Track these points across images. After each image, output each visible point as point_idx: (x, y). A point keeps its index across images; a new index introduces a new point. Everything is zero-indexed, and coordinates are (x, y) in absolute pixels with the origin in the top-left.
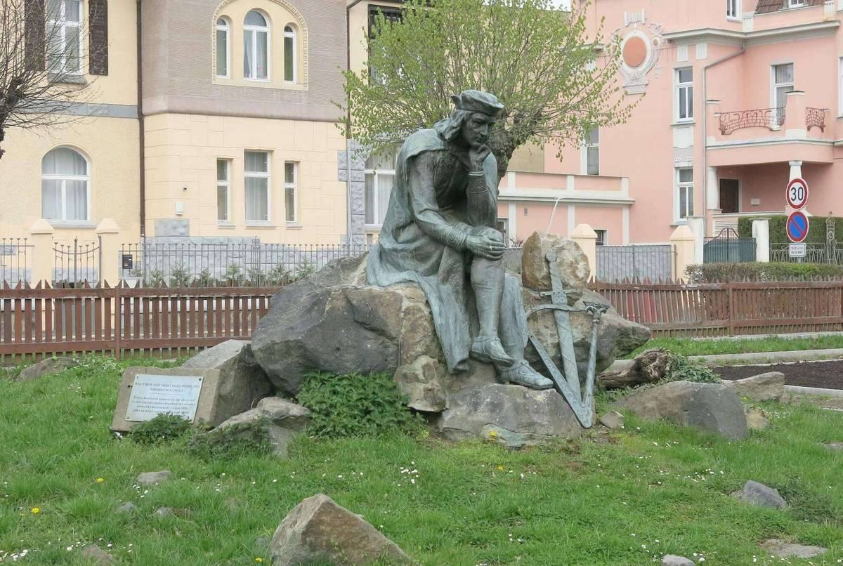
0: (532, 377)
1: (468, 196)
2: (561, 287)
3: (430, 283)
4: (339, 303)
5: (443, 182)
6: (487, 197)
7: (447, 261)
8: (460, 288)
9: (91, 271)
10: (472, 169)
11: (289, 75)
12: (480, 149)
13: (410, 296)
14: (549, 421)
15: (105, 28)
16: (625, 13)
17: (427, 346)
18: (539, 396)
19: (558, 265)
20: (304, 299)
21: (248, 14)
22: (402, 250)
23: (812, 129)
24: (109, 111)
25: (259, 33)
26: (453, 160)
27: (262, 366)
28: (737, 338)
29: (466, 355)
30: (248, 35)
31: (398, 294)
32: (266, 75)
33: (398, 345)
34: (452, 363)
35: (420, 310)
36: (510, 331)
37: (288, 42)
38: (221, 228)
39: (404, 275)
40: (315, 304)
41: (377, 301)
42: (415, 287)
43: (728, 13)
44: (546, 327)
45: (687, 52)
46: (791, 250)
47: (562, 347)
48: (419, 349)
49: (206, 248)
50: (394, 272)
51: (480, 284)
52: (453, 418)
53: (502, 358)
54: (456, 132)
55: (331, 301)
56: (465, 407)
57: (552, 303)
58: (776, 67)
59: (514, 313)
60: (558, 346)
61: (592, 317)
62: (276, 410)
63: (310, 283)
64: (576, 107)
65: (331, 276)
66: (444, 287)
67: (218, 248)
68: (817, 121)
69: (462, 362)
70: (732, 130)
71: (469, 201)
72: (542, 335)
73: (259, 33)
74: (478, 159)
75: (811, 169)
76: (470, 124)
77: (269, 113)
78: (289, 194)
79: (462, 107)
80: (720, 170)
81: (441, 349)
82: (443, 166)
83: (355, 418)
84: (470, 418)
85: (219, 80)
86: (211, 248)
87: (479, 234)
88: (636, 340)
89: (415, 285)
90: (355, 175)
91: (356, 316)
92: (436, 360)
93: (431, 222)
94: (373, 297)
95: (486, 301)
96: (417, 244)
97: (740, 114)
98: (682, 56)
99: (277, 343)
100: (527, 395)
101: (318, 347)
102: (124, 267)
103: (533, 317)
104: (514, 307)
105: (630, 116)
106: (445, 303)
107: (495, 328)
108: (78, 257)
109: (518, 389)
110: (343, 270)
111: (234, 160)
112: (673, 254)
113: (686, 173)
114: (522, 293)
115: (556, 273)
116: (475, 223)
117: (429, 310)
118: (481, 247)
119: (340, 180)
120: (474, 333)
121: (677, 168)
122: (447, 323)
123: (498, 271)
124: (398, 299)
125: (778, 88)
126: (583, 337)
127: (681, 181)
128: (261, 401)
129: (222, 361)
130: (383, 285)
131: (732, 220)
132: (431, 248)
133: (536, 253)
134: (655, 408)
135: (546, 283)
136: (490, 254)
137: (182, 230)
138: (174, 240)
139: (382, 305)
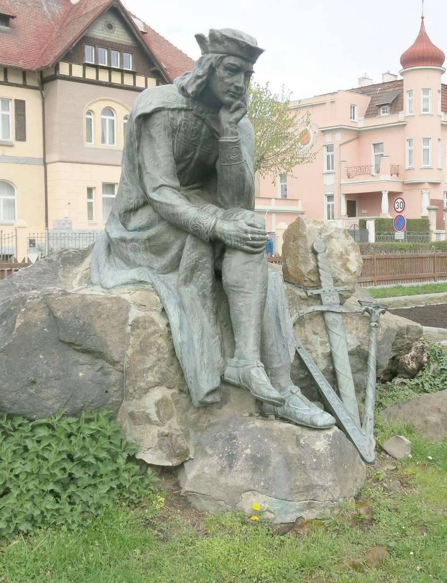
0: (307, 413)
1: (219, 171)
2: (331, 283)
3: (169, 284)
4: (36, 315)
5: (186, 152)
6: (242, 170)
7: (191, 253)
8: (208, 291)
9: (10, 248)
12: (234, 106)
13: (139, 302)
15: (24, 115)
17: (163, 374)
18: (318, 443)
19: (327, 257)
21: (102, 111)
22: (132, 240)
24: (28, 161)
26: (199, 123)
28: (378, 287)
29: (216, 383)
30: (103, 121)
31: (124, 300)
32: (114, 142)
33: (123, 372)
34: (197, 394)
35: (153, 322)
36: (274, 348)
38: (90, 224)
39: (133, 274)
41: (92, 311)
42: (147, 290)
43: (351, 118)
44: (315, 333)
46: (396, 236)
47: (335, 358)
48: (151, 378)
49: (81, 235)
55: (24, 313)
56: (216, 458)
57: (321, 304)
58: (374, 145)
59: (278, 319)
60: (330, 357)
61: (369, 319)
63: (12, 284)
64: (285, 152)
65: (44, 273)
67: (88, 235)
68: (395, 172)
69: (213, 392)
71: (219, 177)
72: (311, 343)
74: (231, 120)
75: (392, 195)
76: (220, 72)
79: (210, 49)
80: (347, 195)
81: (182, 375)
82: (185, 131)
84: (223, 480)
85: (88, 145)
86: (85, 235)
87: (232, 218)
88: (409, 339)
89: (147, 286)
91: (61, 334)
92: (175, 391)
93: (168, 202)
94: (87, 305)
95: (243, 309)
96: (152, 232)
98: (328, 139)
100: (302, 441)
102: (30, 246)
103: (300, 322)
104: (277, 311)
105: (315, 158)
106: (188, 312)
107: (256, 348)
108: (3, 240)
109: (288, 429)
113: (330, 198)
114: (288, 293)
115: (326, 267)
117: (165, 322)
118: (237, 236)
120: (228, 352)
121: (325, 195)
122: (191, 339)
123: (259, 268)
124: (123, 307)
125: (375, 155)
126: (359, 344)
127: (328, 201)
130: (112, 286)
131: (355, 220)
132: (169, 236)
133: (300, 243)
134: (440, 423)
135: (314, 278)
136: (247, 245)
137: (68, 226)
138: (63, 231)
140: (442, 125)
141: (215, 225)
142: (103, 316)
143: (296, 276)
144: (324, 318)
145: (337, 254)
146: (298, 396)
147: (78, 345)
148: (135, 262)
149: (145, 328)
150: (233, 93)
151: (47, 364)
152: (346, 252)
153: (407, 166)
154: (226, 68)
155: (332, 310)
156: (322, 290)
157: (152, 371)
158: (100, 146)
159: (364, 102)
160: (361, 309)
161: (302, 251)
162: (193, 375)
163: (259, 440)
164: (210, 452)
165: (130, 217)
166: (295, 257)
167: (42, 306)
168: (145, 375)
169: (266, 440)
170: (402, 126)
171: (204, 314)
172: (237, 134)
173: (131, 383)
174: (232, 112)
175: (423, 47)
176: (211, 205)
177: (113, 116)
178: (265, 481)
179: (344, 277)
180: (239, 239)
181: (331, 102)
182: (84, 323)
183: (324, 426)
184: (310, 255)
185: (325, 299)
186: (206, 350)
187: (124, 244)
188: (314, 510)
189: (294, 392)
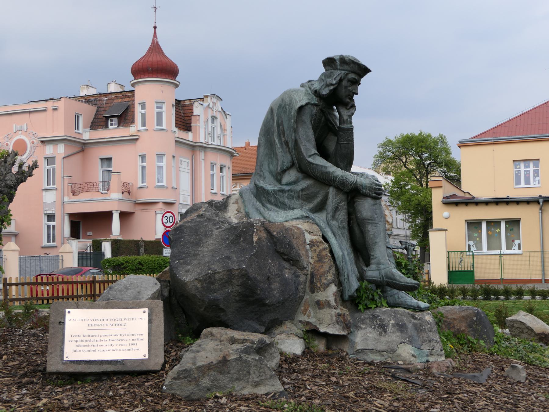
16: (14, 125)
22: (289, 190)
33: (306, 275)
45: (52, 147)
51: (369, 220)
53: (411, 283)
76: (344, 83)
79: (338, 67)
80: (71, 215)
98: (49, 150)
99: (219, 273)
112: (61, 260)
113: (51, 217)
118: (370, 187)
121: (45, 214)
124: (302, 233)
127: (48, 221)
140: (176, 141)
147: (287, 255)
148: (290, 206)
151: (273, 266)
153: (140, 184)
159: (89, 111)
164: (363, 326)
168: (326, 275)
170: (134, 140)
175: (154, 58)
178: (408, 337)
180: (371, 189)
181: (53, 109)
187: (281, 194)
188: (433, 356)
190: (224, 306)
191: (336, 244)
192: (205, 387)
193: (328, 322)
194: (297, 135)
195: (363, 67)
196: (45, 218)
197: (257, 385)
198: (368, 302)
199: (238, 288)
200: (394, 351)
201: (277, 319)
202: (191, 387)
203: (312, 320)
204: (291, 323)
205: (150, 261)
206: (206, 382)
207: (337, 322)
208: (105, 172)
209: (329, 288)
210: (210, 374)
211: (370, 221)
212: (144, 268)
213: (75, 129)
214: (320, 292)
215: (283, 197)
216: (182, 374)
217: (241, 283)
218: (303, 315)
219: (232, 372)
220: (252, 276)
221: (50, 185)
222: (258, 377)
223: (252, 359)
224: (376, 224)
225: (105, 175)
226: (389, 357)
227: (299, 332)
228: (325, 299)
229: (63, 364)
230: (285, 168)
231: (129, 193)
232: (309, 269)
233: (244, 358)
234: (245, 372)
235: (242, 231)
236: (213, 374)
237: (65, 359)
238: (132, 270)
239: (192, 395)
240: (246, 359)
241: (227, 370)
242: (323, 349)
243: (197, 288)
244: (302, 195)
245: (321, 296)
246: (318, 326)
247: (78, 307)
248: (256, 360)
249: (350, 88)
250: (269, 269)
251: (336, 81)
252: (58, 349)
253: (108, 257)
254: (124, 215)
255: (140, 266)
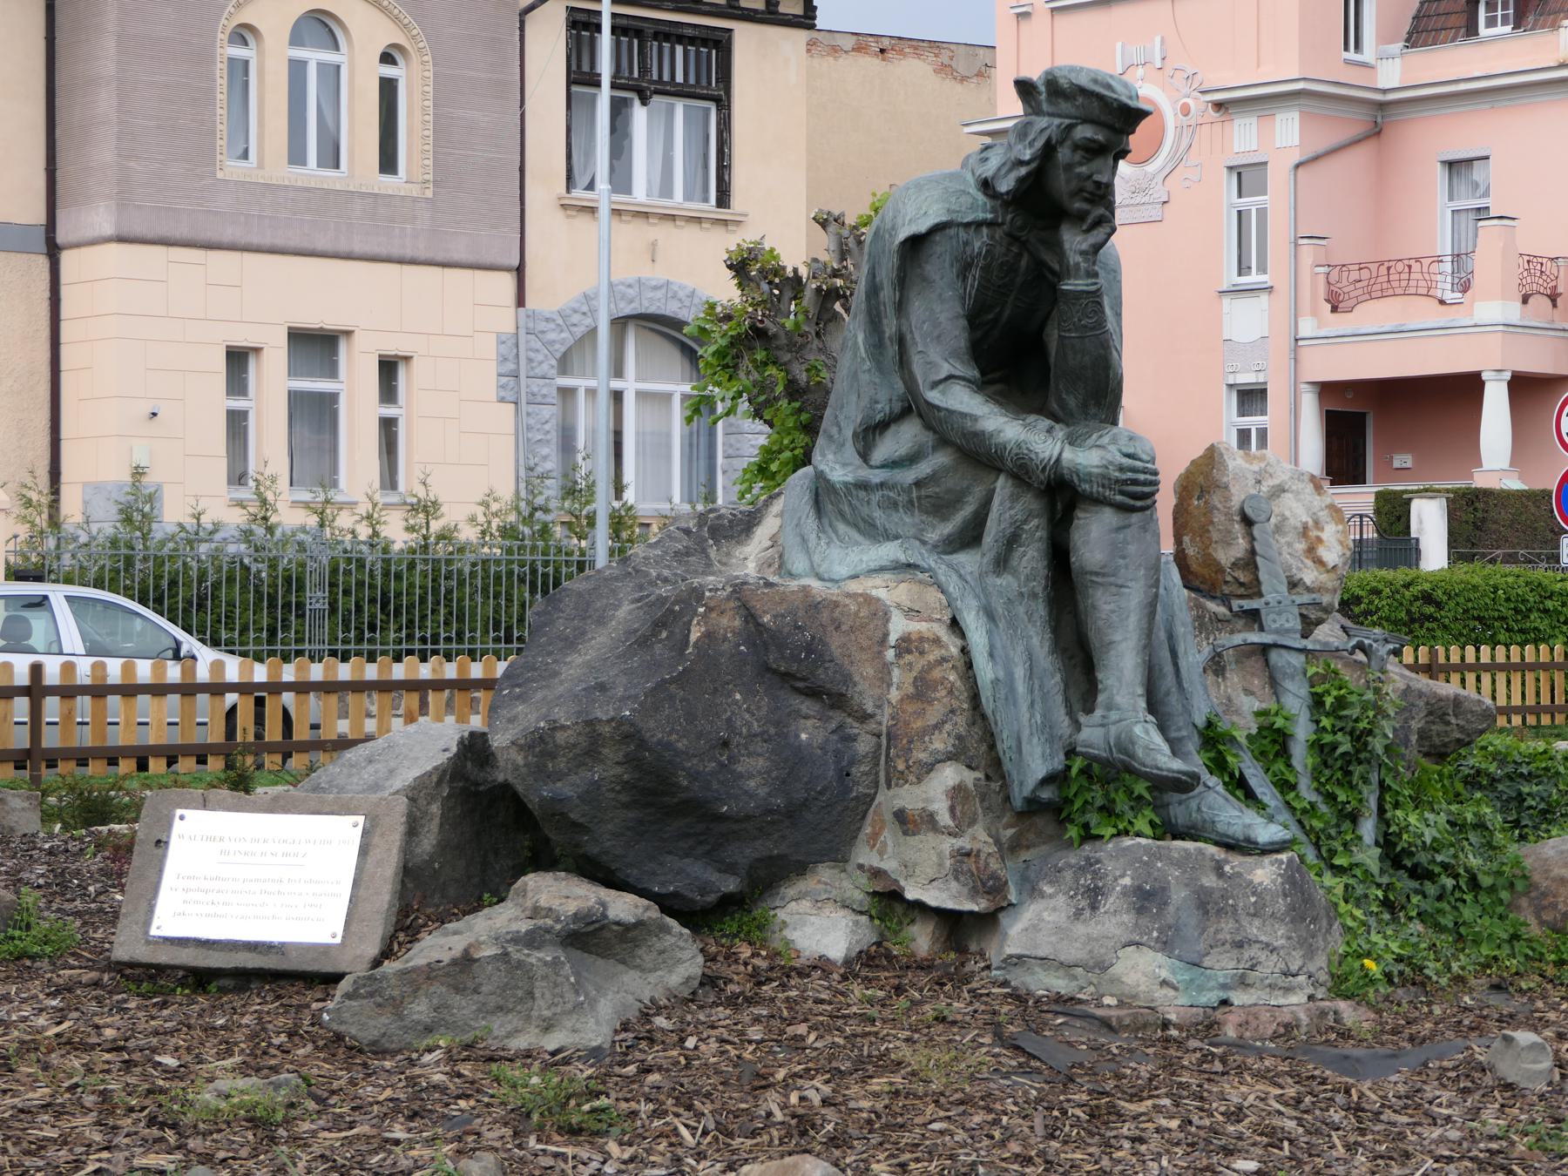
2: (1284, 588)
4: (724, 621)
8: (1039, 586)
10: (1066, 272)
11: (388, 163)
13: (907, 603)
14: (1289, 938)
16: (1119, 45)
17: (959, 738)
18: (1259, 872)
20: (625, 612)
22: (882, 485)
23: (1531, 300)
25: (321, 66)
27: (520, 789)
30: (297, 69)
31: (878, 600)
33: (879, 736)
34: (1021, 784)
35: (937, 641)
37: (388, 89)
39: (889, 551)
40: (659, 624)
41: (825, 615)
45: (1254, 127)
48: (940, 743)
50: (857, 544)
51: (1097, 574)
52: (1034, 928)
53: (1169, 770)
54: (1028, 175)
55: (704, 616)
57: (1262, 629)
58: (1451, 165)
62: (571, 907)
63: (637, 571)
66: (999, 581)
70: (1354, 301)
73: (321, 66)
74: (1084, 247)
75: (1525, 388)
76: (1064, 154)
77: (343, 247)
78: (388, 426)
79: (1045, 107)
80: (1327, 390)
83: (1416, 866)
85: (232, 169)
88: (1461, 728)
90: (535, 389)
92: (979, 775)
96: (924, 469)
97: (1373, 267)
98: (1244, 137)
99: (563, 728)
100: (1227, 868)
101: (674, 737)
103: (1216, 665)
110: (717, 542)
111: (265, 350)
113: (1251, 398)
116: (1072, 415)
118: (1103, 476)
119: (502, 400)
121: (1231, 386)
122: (1010, 675)
124: (881, 614)
127: (1242, 413)
128: (519, 883)
129: (409, 775)
131: (1360, 498)
133: (1216, 500)
135: (1243, 577)
136: (1122, 493)
139: (837, 628)
141: (1060, 454)
142: (844, 628)
143: (1205, 572)
144: (1267, 661)
145: (1296, 528)
146: (1218, 793)
147: (804, 679)
148: (886, 530)
149: (922, 653)
150: (1091, 193)
151: (748, 710)
152: (1317, 523)
154: (1076, 147)
155: (1285, 643)
156: (1263, 600)
157: (941, 732)
158: (279, 171)
160: (1347, 643)
161: (1218, 518)
162: (1014, 745)
163: (1146, 863)
164: (1048, 890)
165: (874, 439)
166: (1204, 531)
167: (732, 604)
168: (927, 739)
169: (1159, 865)
171: (1032, 631)
172: (1096, 275)
173: (900, 753)
174: (1088, 230)
176: (1036, 417)
177: (337, 47)
178: (1160, 931)
179: (1310, 576)
180: (1106, 482)
182: (813, 638)
183: (1272, 843)
184: (1237, 526)
185: (1267, 619)
186: (1038, 700)
187: (862, 494)
188: (1253, 991)
189: (1210, 784)
190: (583, 816)
191: (981, 646)
192: (418, 1022)
193: (931, 873)
194: (903, 321)
195: (1115, 105)
196: (1229, 399)
197: (548, 1027)
198: (1093, 818)
199: (619, 770)
200: (1102, 966)
201: (781, 857)
202: (384, 1020)
203: (889, 865)
204: (836, 871)
205: (1475, 588)
206: (420, 1009)
207: (956, 874)
208: (1463, 216)
209: (932, 775)
210: (432, 989)
211: (1099, 579)
212: (1446, 615)
213: (1346, 48)
214: (907, 786)
215: (868, 503)
216: (365, 985)
217: (625, 756)
218: (867, 849)
219: (484, 989)
220: (655, 739)
221: (1249, 274)
222: (549, 1008)
223: (539, 960)
224: (1117, 586)
225: (1463, 226)
226: (1091, 983)
227: (858, 895)
228: (921, 805)
229: (148, 942)
230: (879, 417)
231: (1553, 298)
232: (885, 718)
233: (516, 956)
234: (520, 993)
235: (670, 610)
236: (439, 991)
237: (154, 932)
238: (1396, 622)
239: (383, 1040)
240: (523, 958)
241: (470, 985)
242: (926, 948)
243: (516, 768)
244: (919, 498)
245: (908, 797)
246: (902, 883)
247: (205, 805)
248: (546, 963)
249: (1083, 169)
250: (729, 720)
251: (1033, 150)
252: (143, 906)
253: (1437, 567)
254: (1525, 388)
255: (1429, 610)
